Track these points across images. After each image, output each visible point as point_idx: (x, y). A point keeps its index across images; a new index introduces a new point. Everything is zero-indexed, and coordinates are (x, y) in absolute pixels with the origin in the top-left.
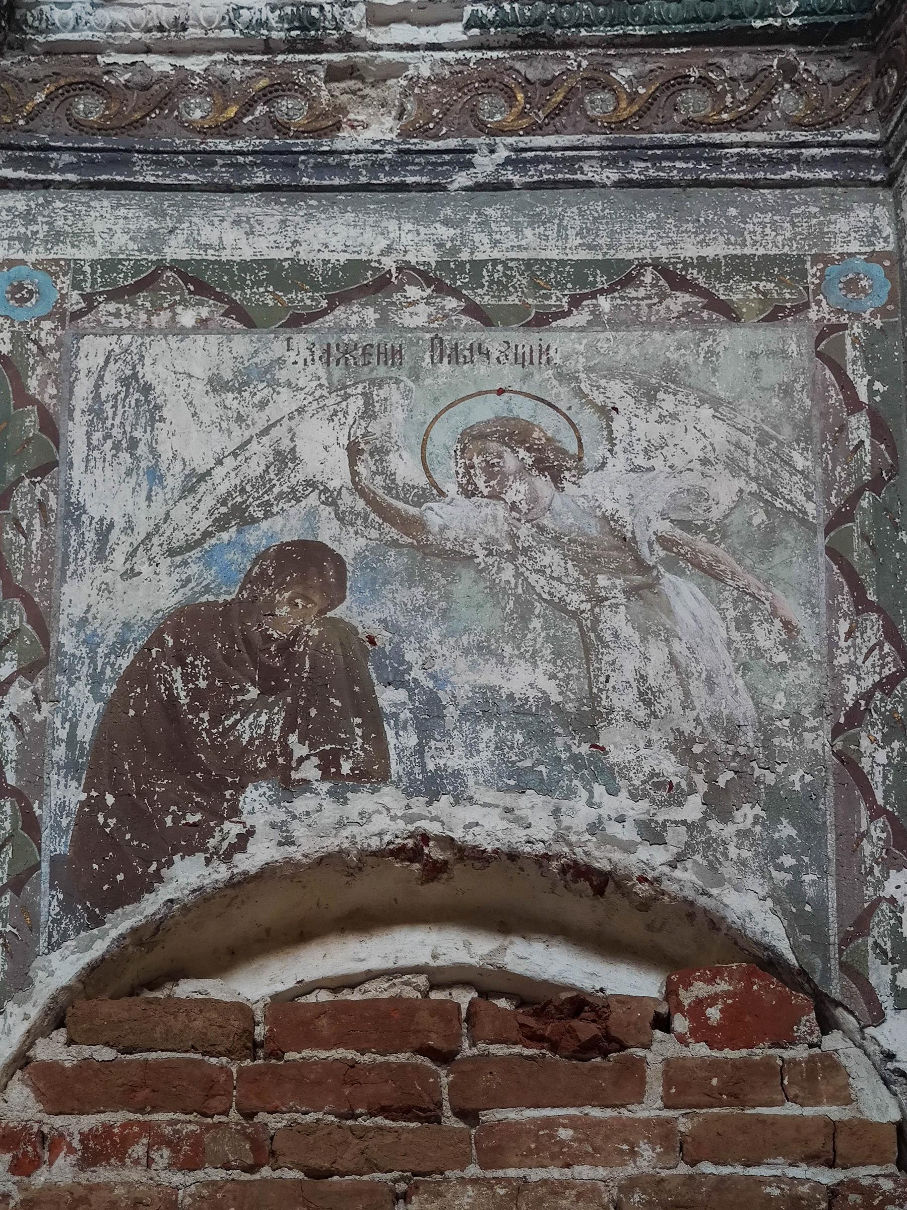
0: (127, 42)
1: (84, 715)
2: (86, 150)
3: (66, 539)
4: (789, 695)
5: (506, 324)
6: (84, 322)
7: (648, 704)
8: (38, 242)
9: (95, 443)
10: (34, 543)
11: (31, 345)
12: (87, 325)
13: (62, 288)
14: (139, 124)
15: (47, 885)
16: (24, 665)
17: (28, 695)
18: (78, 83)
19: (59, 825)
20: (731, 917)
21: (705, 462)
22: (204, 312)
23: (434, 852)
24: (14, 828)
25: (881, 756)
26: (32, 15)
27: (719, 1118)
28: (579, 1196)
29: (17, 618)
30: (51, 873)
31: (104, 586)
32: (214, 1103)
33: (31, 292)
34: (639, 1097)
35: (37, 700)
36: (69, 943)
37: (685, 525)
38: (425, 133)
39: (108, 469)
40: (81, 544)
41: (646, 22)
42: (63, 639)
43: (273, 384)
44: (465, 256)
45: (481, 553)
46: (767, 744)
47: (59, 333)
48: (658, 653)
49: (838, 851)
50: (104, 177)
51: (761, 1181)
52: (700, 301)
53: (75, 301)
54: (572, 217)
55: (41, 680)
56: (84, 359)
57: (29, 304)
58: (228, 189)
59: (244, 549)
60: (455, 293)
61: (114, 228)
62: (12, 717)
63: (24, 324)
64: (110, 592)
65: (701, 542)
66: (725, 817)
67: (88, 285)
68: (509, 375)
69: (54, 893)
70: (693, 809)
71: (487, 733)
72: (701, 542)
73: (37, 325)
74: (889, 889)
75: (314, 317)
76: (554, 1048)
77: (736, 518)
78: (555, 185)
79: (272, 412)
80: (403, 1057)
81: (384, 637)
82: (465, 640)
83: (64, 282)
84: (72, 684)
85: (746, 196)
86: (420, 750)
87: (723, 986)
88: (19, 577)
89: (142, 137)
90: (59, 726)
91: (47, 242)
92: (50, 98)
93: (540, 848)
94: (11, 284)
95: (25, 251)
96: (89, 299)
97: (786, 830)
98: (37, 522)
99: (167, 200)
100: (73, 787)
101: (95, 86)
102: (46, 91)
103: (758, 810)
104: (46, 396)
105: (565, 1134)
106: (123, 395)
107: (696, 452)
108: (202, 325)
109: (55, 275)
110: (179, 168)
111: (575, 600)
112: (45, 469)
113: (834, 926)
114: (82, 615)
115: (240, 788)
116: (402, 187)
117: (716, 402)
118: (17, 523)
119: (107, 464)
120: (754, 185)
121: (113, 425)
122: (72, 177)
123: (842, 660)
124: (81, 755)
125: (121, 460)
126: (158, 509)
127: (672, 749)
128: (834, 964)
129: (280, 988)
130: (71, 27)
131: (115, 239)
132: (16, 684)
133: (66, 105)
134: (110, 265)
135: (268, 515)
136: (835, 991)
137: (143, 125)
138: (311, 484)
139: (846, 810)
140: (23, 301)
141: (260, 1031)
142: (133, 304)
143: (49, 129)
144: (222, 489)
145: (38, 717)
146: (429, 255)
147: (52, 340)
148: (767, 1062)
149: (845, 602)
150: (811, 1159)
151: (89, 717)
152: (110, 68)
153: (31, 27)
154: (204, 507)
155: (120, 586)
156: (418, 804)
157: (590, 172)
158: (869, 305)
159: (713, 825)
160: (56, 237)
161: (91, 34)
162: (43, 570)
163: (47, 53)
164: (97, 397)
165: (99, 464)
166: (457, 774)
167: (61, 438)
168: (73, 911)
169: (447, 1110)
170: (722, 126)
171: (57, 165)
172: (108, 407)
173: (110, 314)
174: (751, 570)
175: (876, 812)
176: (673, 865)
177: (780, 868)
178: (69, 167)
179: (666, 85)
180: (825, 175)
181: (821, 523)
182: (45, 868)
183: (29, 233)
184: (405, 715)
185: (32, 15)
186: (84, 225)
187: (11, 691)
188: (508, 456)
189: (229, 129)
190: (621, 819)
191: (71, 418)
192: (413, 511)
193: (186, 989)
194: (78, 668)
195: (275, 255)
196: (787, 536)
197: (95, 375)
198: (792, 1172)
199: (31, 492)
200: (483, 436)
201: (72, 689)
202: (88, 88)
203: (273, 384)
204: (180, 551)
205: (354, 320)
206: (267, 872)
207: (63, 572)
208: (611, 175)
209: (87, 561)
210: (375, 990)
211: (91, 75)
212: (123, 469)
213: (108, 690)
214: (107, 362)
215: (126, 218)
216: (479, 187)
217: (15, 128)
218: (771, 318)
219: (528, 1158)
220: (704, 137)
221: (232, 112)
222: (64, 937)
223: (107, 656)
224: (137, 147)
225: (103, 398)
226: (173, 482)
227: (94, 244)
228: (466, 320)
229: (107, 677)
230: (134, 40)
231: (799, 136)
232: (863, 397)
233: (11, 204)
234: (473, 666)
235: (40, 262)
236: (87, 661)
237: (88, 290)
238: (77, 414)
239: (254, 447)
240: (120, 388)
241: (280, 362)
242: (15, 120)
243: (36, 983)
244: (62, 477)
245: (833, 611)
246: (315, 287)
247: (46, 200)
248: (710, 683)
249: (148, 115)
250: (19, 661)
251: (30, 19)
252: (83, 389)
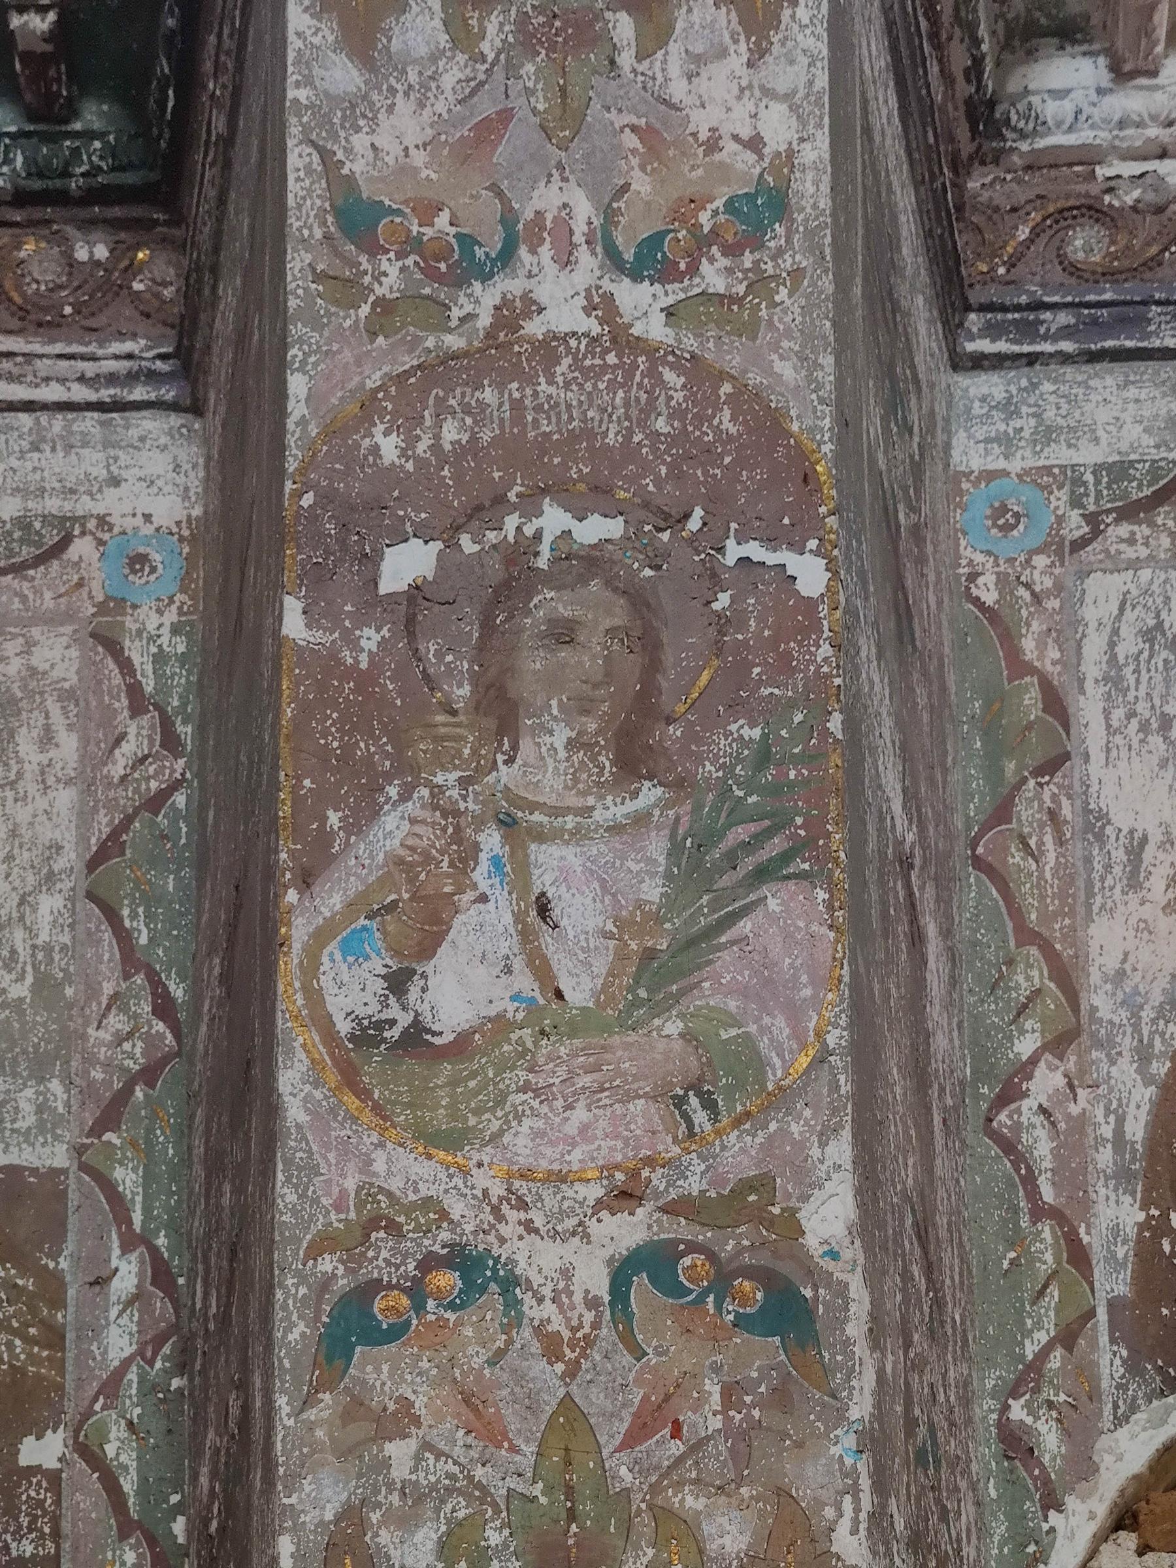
0: (1138, 143)
1: (1133, 1105)
2: (1088, 305)
3: (1088, 860)
6: (1090, 553)
8: (1023, 443)
9: (1115, 723)
10: (1047, 868)
11: (1022, 592)
12: (1092, 558)
13: (1057, 508)
14: (1156, 262)
15: (1106, 1338)
16: (1049, 1037)
17: (1059, 1080)
18: (1071, 209)
19: (1114, 1255)
24: (1058, 1261)
26: (1018, 112)
29: (1035, 973)
30: (1110, 1321)
31: (1142, 925)
33: (1017, 516)
35: (1071, 1086)
36: (1138, 1416)
39: (1136, 760)
40: (1108, 867)
42: (1097, 1001)
47: (1057, 571)
50: (1109, 344)
53: (1076, 526)
55: (1073, 1058)
56: (1091, 607)
57: (1015, 532)
61: (1123, 416)
62: (1042, 1110)
63: (1011, 561)
64: (1150, 933)
67: (1092, 499)
69: (1115, 1348)
73: (1028, 561)
83: (1060, 499)
84: (1113, 1063)
88: (1033, 916)
89: (1160, 281)
90: (1102, 1121)
91: (1035, 442)
92: (1036, 233)
94: (992, 506)
95: (1006, 458)
96: (1092, 519)
98: (1048, 839)
100: (1126, 1204)
101: (1094, 211)
102: (1031, 224)
104: (1048, 662)
106: (1146, 654)
109: (1047, 488)
112: (1053, 765)
114: (1118, 966)
118: (1023, 841)
119: (1133, 753)
121: (1136, 697)
122: (1067, 346)
124: (1133, 1160)
125: (1152, 747)
130: (1065, 126)
131: (1124, 431)
132: (1042, 1064)
133: (1056, 242)
134: (1118, 471)
137: (1160, 264)
140: (1007, 528)
142: (1152, 524)
143: (1038, 278)
145: (1074, 1110)
147: (1048, 583)
151: (1138, 1107)
152: (1112, 183)
153: (1014, 129)
160: (1047, 435)
161: (1092, 134)
162: (1062, 906)
163: (1029, 168)
164: (1113, 658)
165: (1124, 753)
167: (1072, 719)
168: (1142, 1373)
171: (1048, 329)
172: (1128, 672)
173: (1122, 541)
178: (1066, 332)
182: (1102, 1315)
183: (1011, 431)
185: (1018, 112)
186: (1082, 414)
187: (1037, 1074)
191: (1082, 691)
194: (1118, 1040)
197: (1108, 629)
199: (1038, 797)
201: (1114, 1069)
202: (1083, 215)
207: (1089, 906)
209: (1117, 891)
211: (1087, 195)
212: (1155, 760)
213: (1160, 1068)
214: (1122, 609)
215: (1137, 401)
217: (993, 280)
222: (1133, 1408)
223: (1154, 1021)
224: (1157, 296)
225: (1122, 661)
227: (1096, 440)
229: (1156, 1051)
230: (1149, 140)
233: (985, 390)
235: (1027, 472)
236: (1129, 1030)
237: (1092, 508)
238: (1089, 685)
240: (1141, 645)
242: (993, 269)
243: (1102, 1470)
244: (1077, 776)
247: (1032, 384)
249: (1166, 249)
250: (1043, 1032)
251: (1014, 117)
252: (1094, 647)
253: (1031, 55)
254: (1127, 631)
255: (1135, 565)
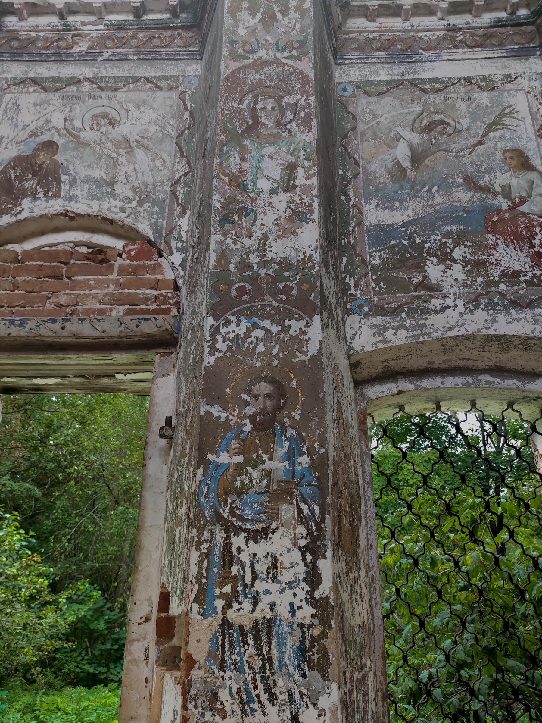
4: (161, 177)
5: (107, 90)
6: (7, 91)
7: (127, 179)
20: (140, 230)
21: (149, 123)
22: (36, 88)
23: (70, 214)
25: (182, 191)
27: (130, 278)
28: (93, 297)
32: (6, 275)
34: (111, 273)
37: (142, 137)
38: (93, 48)
41: (146, 25)
43: (49, 104)
44: (99, 75)
45: (92, 144)
46: (155, 189)
48: (131, 167)
49: (168, 214)
51: (139, 294)
52: (154, 86)
54: (126, 67)
58: (45, 61)
59: (35, 142)
60: (96, 84)
65: (145, 141)
66: (141, 206)
68: (106, 102)
70: (134, 204)
71: (87, 186)
72: (145, 141)
74: (179, 223)
75: (61, 89)
76: (94, 261)
77: (155, 136)
78: (122, 60)
79: (47, 111)
80: (55, 264)
81: (65, 163)
82: (85, 164)
85: (167, 62)
86: (69, 190)
87: (136, 246)
93: (95, 214)
96: (9, 86)
97: (156, 209)
99: (31, 64)
101: (17, 39)
103: (150, 204)
105: (91, 282)
107: (147, 120)
108: (35, 91)
110: (33, 57)
111: (113, 155)
113: (164, 232)
115: (23, 199)
116: (86, 60)
117: (154, 109)
120: (170, 60)
122: (9, 59)
123: (176, 169)
126: (16, 133)
127: (131, 190)
128: (163, 241)
129: (35, 246)
134: (15, 78)
135: (42, 134)
136: (162, 248)
138: (54, 127)
139: (171, 204)
141: (20, 257)
144: (32, 129)
146: (91, 75)
148: (144, 265)
149: (179, 155)
150: (152, 288)
154: (27, 133)
155: (3, 151)
156: (67, 203)
157: (131, 57)
158: (193, 87)
159: (138, 208)
166: (77, 196)
169: (64, 277)
170: (162, 47)
174: (156, 148)
175: (179, 204)
176: (126, 218)
177: (153, 218)
178: (8, 57)
179: (150, 38)
180: (186, 57)
181: (175, 137)
184: (67, 182)
188: (103, 121)
189: (47, 48)
190: (115, 207)
192: (77, 133)
193: (9, 247)
195: (54, 75)
196: (167, 140)
198: (147, 292)
200: (97, 116)
203: (49, 104)
204: (20, 143)
205: (71, 90)
206: (26, 219)
208: (136, 58)
210: (60, 247)
216: (104, 60)
218: (170, 90)
219: (82, 288)
220: (157, 50)
221: (48, 45)
226: (20, 127)
228: (97, 90)
231: (179, 49)
232: (189, 108)
234: (86, 170)
239: (41, 119)
241: (51, 99)
245: (175, 157)
246: (63, 82)
248: (143, 174)
253: (6, 16)
254: (10, 103)
255: (14, 93)
